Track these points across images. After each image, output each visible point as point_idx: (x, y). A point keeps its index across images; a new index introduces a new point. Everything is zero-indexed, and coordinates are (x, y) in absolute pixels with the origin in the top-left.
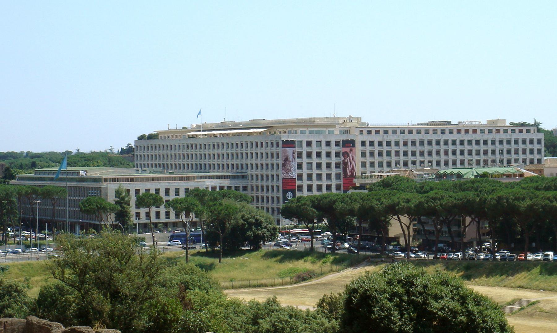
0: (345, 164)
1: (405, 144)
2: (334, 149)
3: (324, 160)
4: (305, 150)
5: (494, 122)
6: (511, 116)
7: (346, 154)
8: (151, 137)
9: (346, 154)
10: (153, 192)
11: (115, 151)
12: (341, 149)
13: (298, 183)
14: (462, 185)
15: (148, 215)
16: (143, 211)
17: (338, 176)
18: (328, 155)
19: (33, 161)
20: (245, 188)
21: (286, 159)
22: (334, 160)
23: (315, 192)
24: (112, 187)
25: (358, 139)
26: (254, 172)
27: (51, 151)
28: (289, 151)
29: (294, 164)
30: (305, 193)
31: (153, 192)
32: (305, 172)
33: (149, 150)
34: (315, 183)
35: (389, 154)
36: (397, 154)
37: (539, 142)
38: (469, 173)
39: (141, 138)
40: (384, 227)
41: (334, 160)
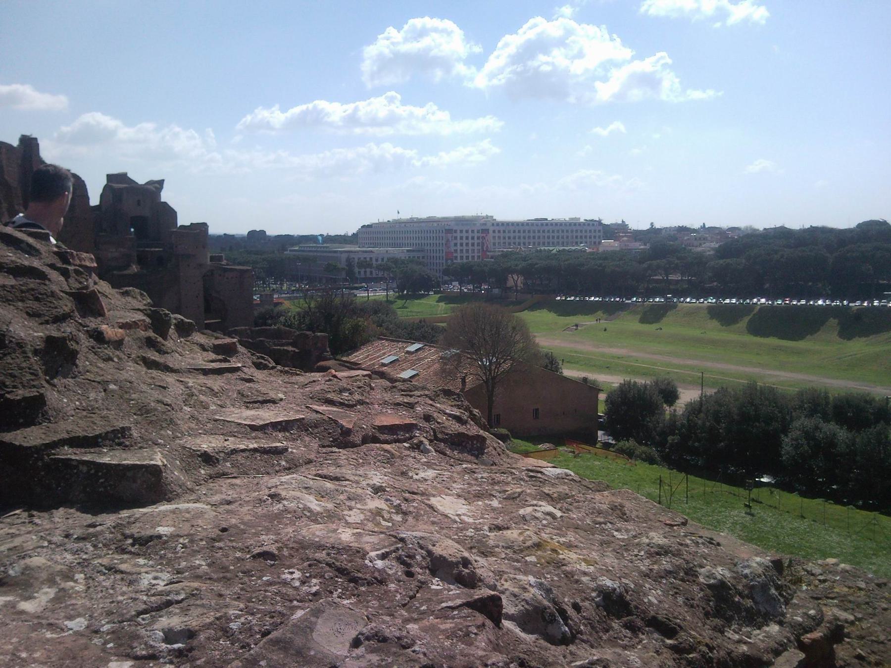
0: (483, 244)
1: (499, 231)
2: (476, 235)
3: (470, 241)
4: (458, 235)
5: (572, 219)
6: (584, 215)
7: (483, 238)
8: (369, 226)
9: (483, 238)
10: (368, 259)
11: (350, 234)
12: (480, 235)
13: (455, 255)
14: (549, 256)
15: (365, 272)
16: (362, 271)
17: (479, 251)
18: (473, 238)
19: (312, 239)
20: (423, 257)
21: (448, 241)
22: (476, 241)
23: (465, 261)
24: (344, 256)
25: (491, 229)
26: (428, 248)
27: (818, 223)
28: (449, 235)
29: (452, 244)
30: (459, 261)
31: (368, 259)
32: (459, 248)
33: (370, 233)
34: (465, 255)
35: (524, 238)
36: (519, 238)
37: (599, 231)
38: (555, 249)
39: (363, 227)
40: (506, 279)
41: (476, 241)
